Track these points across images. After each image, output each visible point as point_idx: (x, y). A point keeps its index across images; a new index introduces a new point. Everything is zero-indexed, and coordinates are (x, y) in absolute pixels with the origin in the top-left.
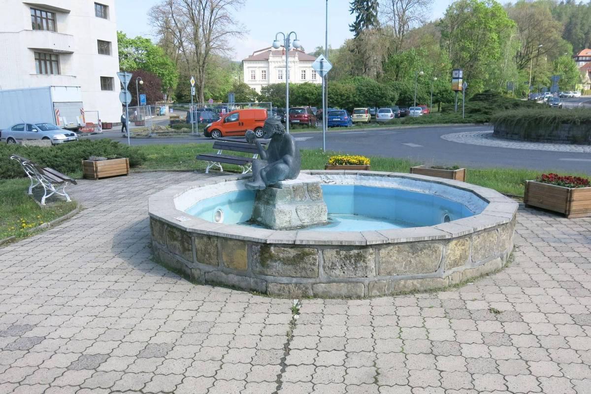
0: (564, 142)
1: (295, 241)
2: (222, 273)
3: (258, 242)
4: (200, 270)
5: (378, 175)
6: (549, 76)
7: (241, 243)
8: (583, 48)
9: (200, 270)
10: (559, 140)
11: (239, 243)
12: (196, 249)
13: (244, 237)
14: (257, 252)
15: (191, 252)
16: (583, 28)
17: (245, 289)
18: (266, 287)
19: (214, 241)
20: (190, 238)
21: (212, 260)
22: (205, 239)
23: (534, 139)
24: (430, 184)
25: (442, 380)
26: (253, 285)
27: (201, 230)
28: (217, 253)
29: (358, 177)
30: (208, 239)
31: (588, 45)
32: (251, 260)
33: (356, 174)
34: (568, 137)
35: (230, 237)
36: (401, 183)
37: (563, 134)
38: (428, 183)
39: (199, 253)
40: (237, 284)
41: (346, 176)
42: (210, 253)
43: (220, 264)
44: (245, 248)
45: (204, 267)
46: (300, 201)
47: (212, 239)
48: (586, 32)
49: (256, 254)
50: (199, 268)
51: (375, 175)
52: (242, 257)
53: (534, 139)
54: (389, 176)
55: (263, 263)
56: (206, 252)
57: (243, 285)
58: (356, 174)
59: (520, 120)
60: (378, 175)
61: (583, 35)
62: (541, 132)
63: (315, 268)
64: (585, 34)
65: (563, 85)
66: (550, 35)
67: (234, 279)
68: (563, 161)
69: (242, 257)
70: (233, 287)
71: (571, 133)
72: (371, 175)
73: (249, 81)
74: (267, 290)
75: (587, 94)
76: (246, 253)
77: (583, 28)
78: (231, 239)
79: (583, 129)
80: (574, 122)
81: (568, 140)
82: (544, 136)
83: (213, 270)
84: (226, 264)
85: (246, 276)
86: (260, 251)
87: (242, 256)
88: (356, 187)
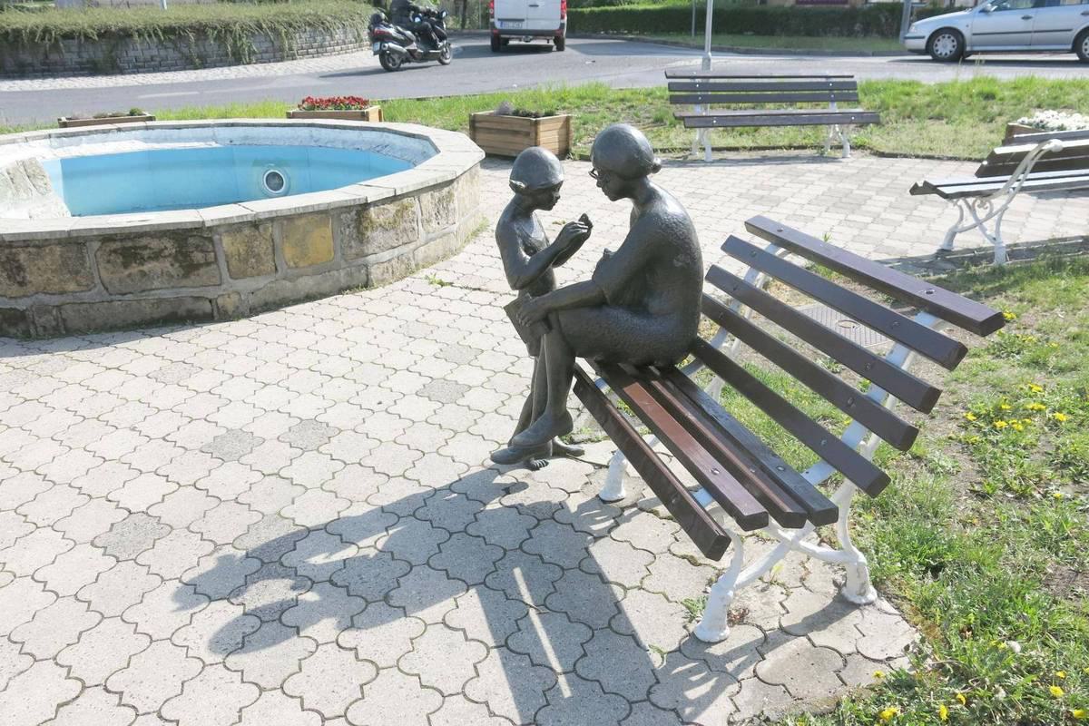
0: (140, 70)
1: (367, 200)
2: (284, 282)
3: (351, 206)
4: (239, 293)
5: (97, 132)
7: (320, 216)
9: (239, 293)
10: (65, 70)
11: (317, 218)
12: (227, 256)
13: (329, 204)
14: (350, 222)
15: (214, 266)
17: (331, 292)
18: (367, 275)
19: (265, 229)
20: (211, 240)
21: (263, 265)
22: (247, 231)
23: (13, 72)
24: (210, 129)
25: (153, 570)
26: (343, 281)
27: (238, 217)
28: (274, 250)
29: (55, 142)
30: (253, 229)
32: (338, 242)
33: (50, 136)
34: (80, 63)
35: (301, 211)
36: (146, 140)
37: (71, 58)
38: (206, 129)
39: (234, 262)
40: (315, 290)
41: (31, 142)
42: (259, 255)
43: (279, 268)
44: (328, 223)
45: (245, 285)
46: (28, 199)
47: (261, 228)
49: (349, 227)
50: (232, 290)
51: (90, 132)
52: (322, 241)
53: (13, 72)
54: (119, 130)
55: (361, 238)
56: (250, 252)
57: (326, 287)
58: (50, 136)
60: (97, 132)
62: (26, 57)
63: (415, 225)
67: (306, 284)
69: (322, 241)
70: (309, 298)
71: (85, 56)
72: (83, 134)
74: (368, 279)
76: (329, 232)
78: (301, 215)
79: (104, 47)
80: (87, 37)
81: (82, 69)
83: (266, 282)
84: (292, 264)
85: (329, 272)
86: (356, 220)
87: (324, 237)
88: (64, 162)
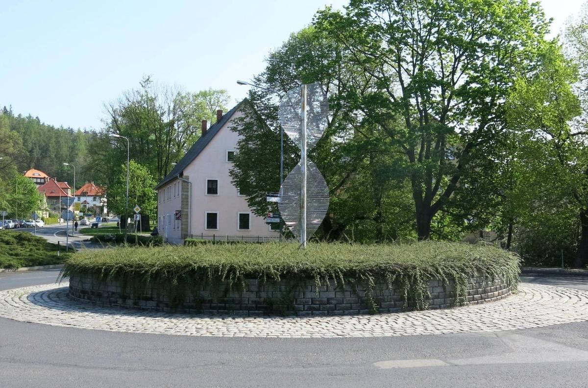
6: (7, 198)
8: (29, 169)
10: (241, 309)
16: (26, 144)
23: (190, 307)
31: (33, 165)
48: (30, 149)
53: (190, 307)
59: (158, 273)
61: (27, 152)
64: (30, 152)
65: (22, 211)
66: (6, 146)
68: (397, 372)
71: (263, 295)
73: (271, 98)
75: (48, 224)
77: (26, 144)
81: (257, 308)
82: (210, 301)
